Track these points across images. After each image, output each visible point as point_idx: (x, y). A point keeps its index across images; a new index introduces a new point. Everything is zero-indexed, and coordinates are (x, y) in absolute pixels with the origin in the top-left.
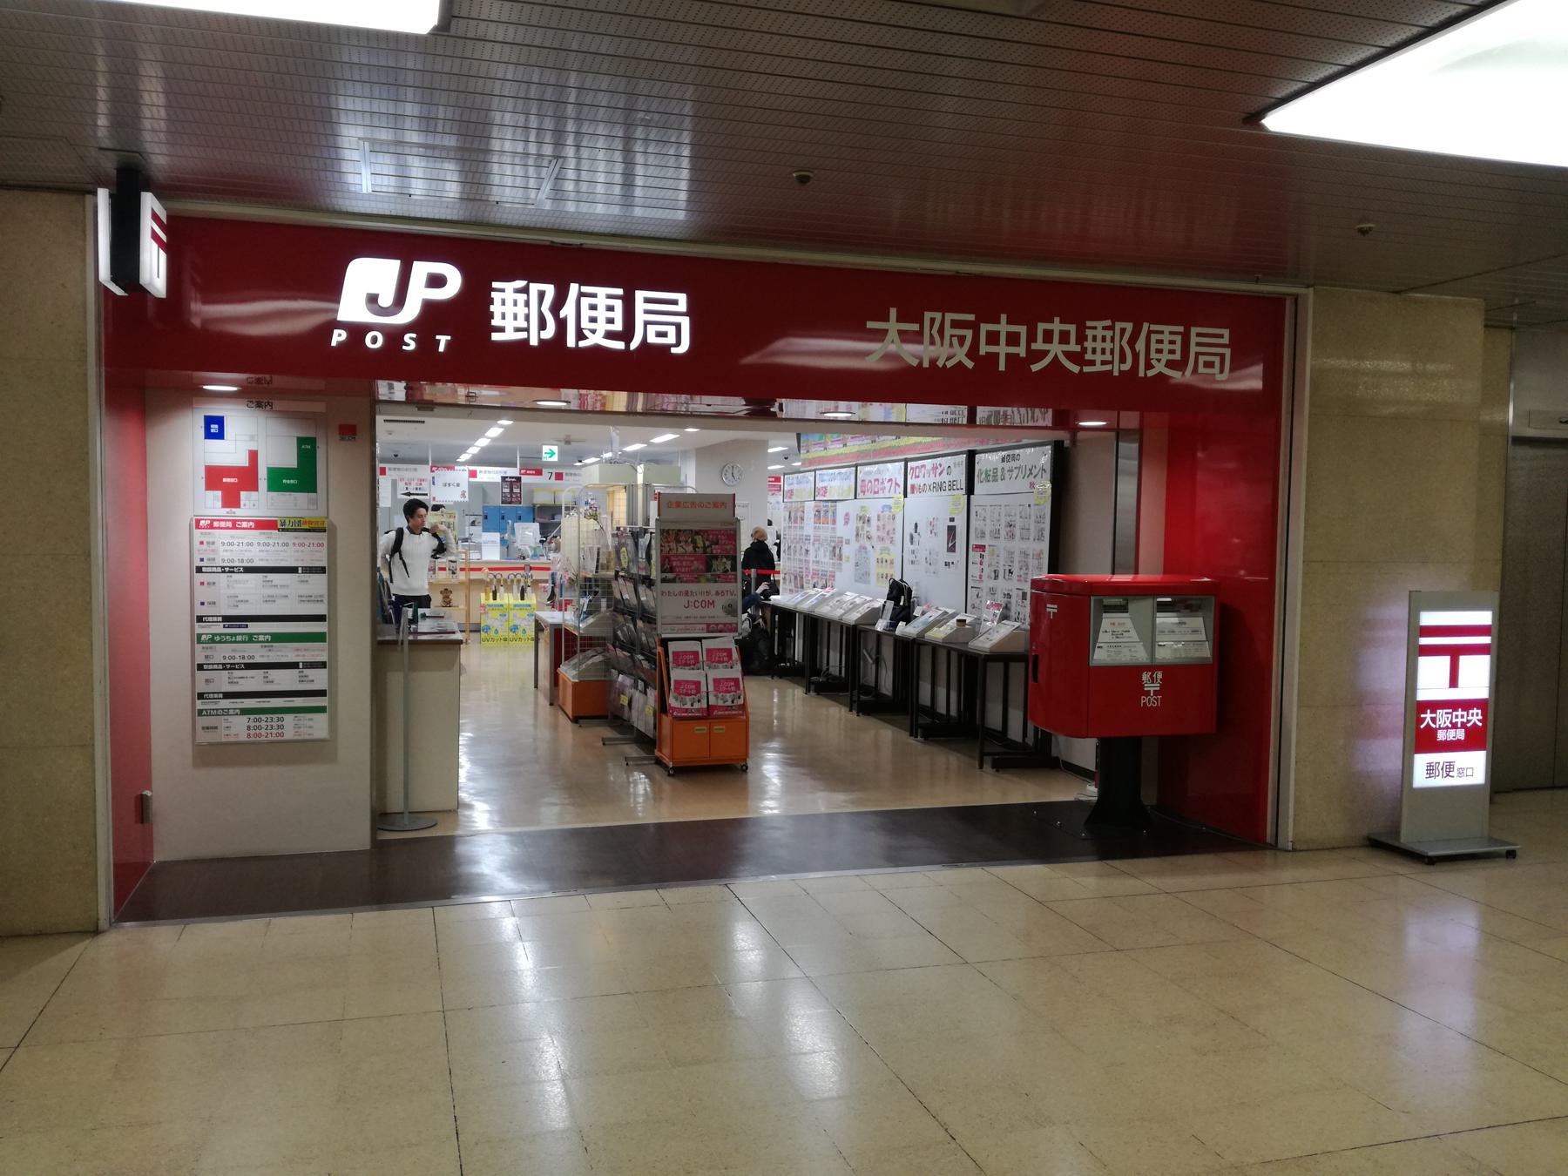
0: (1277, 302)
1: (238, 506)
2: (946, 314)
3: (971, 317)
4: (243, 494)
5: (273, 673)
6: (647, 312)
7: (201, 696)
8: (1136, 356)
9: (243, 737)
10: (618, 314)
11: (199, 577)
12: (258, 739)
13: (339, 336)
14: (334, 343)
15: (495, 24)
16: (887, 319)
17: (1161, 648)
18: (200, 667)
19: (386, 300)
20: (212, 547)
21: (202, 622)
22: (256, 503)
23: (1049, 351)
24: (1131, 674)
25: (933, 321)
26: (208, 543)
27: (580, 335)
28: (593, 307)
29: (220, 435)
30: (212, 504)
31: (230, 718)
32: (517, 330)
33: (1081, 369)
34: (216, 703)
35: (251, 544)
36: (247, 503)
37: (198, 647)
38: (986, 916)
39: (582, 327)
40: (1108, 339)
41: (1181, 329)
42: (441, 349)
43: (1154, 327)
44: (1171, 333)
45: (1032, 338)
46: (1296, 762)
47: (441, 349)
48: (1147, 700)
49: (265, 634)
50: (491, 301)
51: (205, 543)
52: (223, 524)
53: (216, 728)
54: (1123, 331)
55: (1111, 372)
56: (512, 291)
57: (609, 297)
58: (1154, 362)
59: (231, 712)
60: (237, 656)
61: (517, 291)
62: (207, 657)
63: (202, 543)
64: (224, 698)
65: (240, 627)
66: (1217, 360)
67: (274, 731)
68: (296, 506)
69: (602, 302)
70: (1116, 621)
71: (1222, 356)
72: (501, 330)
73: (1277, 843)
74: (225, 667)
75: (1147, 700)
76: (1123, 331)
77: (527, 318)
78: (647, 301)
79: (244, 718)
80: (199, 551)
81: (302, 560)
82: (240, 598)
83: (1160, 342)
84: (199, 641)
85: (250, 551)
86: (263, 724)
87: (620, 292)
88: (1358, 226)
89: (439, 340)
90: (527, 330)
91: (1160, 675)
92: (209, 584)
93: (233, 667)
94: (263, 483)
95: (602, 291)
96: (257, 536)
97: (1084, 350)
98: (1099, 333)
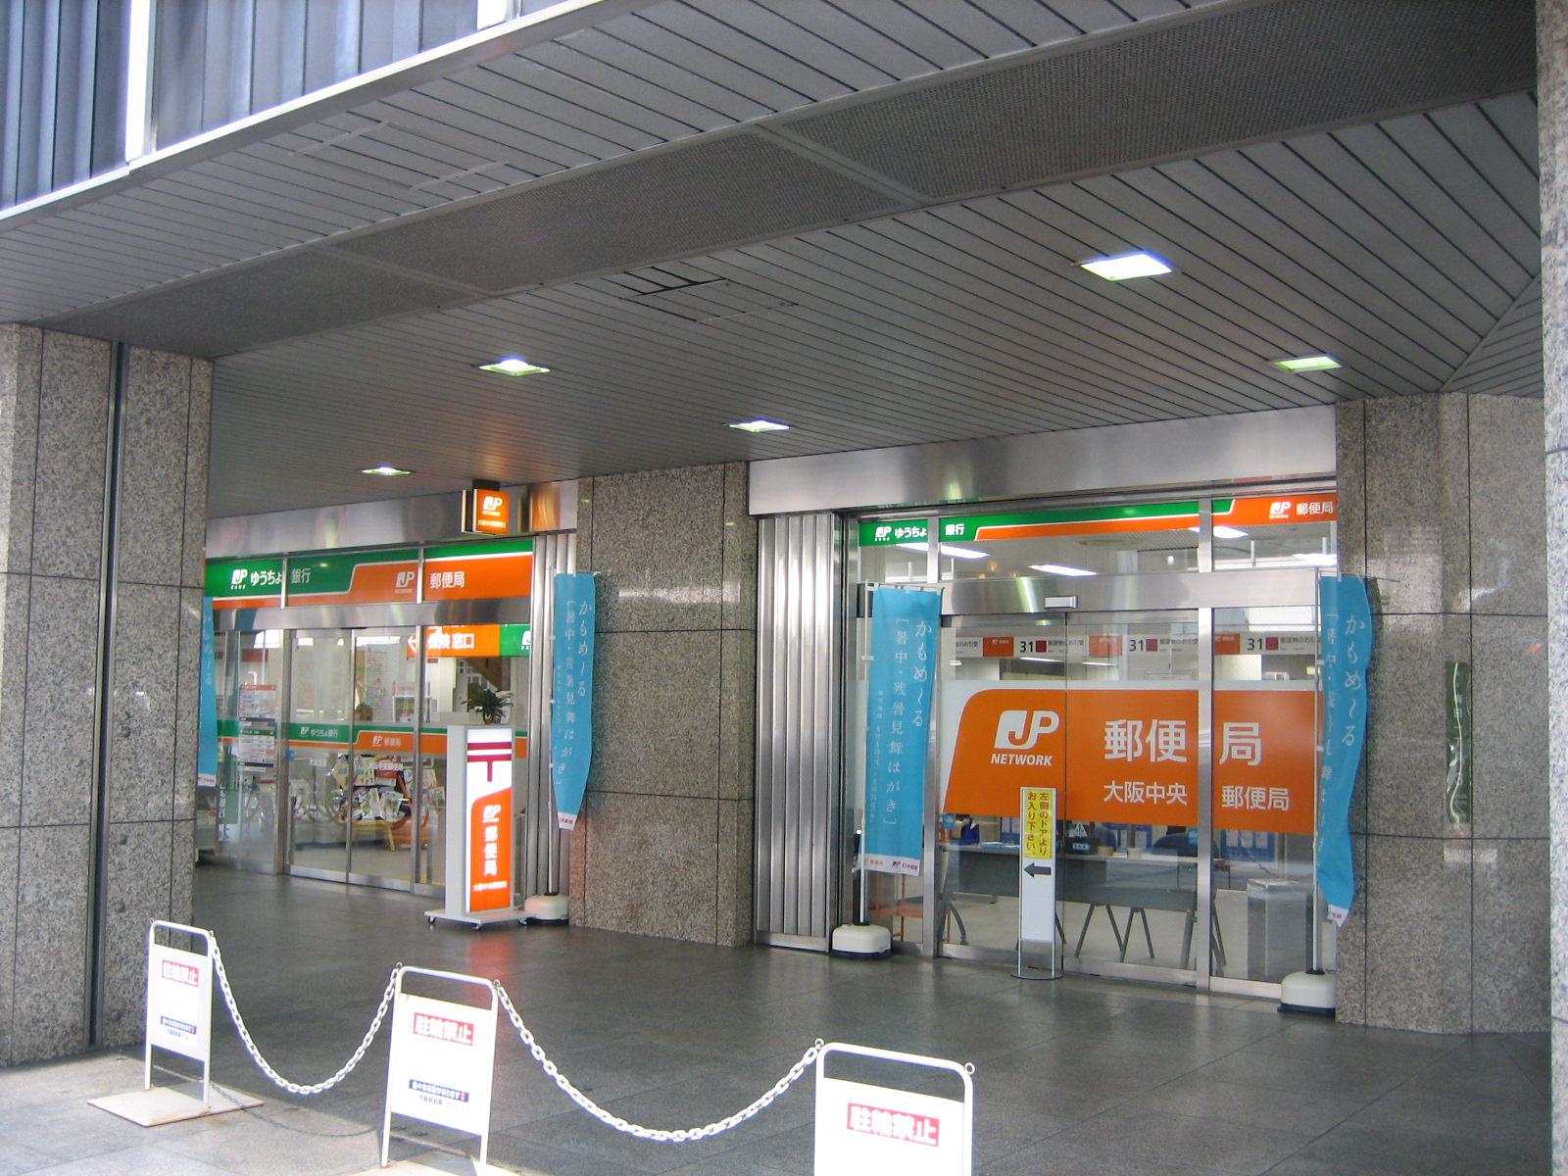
3: (1142, 783)
6: (1231, 737)
19: (1019, 736)
27: (1251, 804)
28: (1166, 734)
45: (1167, 791)
50: (1105, 734)
57: (1177, 727)
61: (1120, 726)
69: (1172, 730)
71: (1285, 801)
77: (1126, 744)
78: (1232, 729)
90: (1126, 751)
95: (1172, 723)
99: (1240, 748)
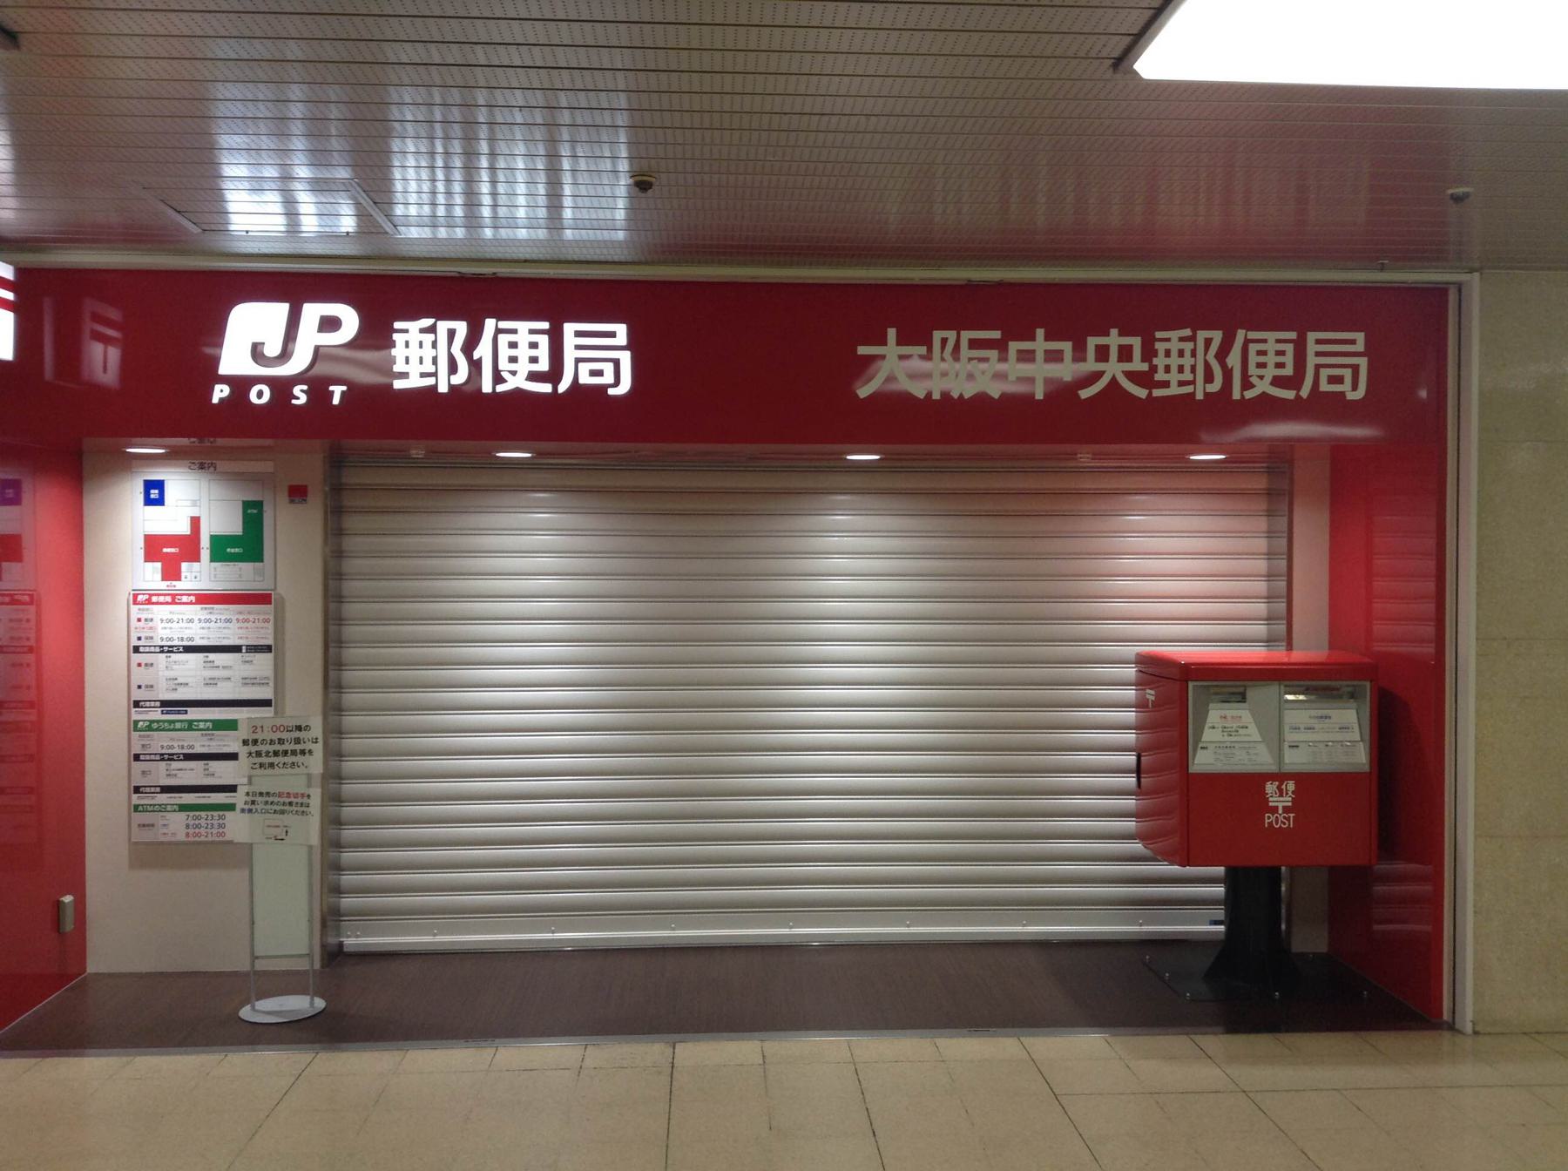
0: (1438, 294)
1: (179, 579)
2: (962, 333)
3: (996, 335)
4: (184, 566)
5: (215, 765)
6: (578, 347)
7: (137, 790)
8: (1228, 374)
9: (181, 837)
10: (543, 352)
11: (136, 658)
12: (197, 839)
13: (220, 392)
14: (215, 400)
15: (743, 54)
16: (883, 342)
17: (1202, 751)
18: (137, 758)
19: (273, 349)
20: (150, 624)
21: (139, 707)
22: (198, 575)
23: (1104, 372)
24: (1247, 786)
25: (944, 341)
26: (146, 620)
27: (498, 378)
29: (160, 501)
30: (150, 576)
31: (168, 815)
32: (423, 375)
33: (1150, 393)
34: (153, 798)
35: (191, 621)
36: (188, 574)
37: (135, 735)
38: (1143, 1093)
39: (500, 368)
40: (1188, 353)
41: (1293, 335)
42: (336, 400)
44: (1278, 341)
46: (1475, 912)
47: (336, 400)
48: (1273, 818)
49: (206, 721)
51: (143, 620)
52: (161, 599)
53: (153, 825)
54: (1208, 342)
55: (1193, 394)
56: (418, 331)
57: (532, 332)
58: (1254, 380)
59: (169, 808)
60: (176, 745)
61: (423, 331)
62: (143, 746)
63: (139, 620)
64: (162, 792)
65: (179, 713)
66: (1347, 373)
67: (214, 831)
68: (240, 576)
69: (523, 338)
70: (1229, 713)
72: (404, 375)
73: (1454, 1023)
74: (162, 757)
75: (1273, 818)
76: (1208, 342)
77: (435, 361)
78: (579, 334)
79: (183, 815)
80: (136, 628)
81: (247, 638)
82: (180, 681)
83: (513, 345)
84: (136, 729)
85: (229, 628)
86: (203, 822)
87: (545, 325)
88: (1450, 192)
89: (333, 392)
90: (435, 375)
91: (1291, 786)
92: (146, 665)
93: (171, 758)
94: (205, 554)
95: (523, 326)
96: (197, 611)
97: (1154, 369)
98: (1175, 346)
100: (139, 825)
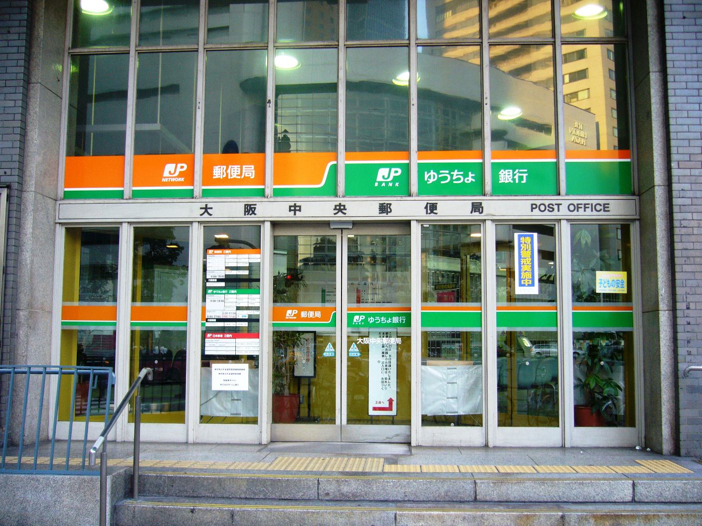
10: (239, 171)
19: (386, 177)
27: (231, 176)
41: (239, 166)
43: (233, 166)
50: (213, 170)
69: (236, 169)
95: (236, 166)
99: (248, 173)
100: (244, 370)
